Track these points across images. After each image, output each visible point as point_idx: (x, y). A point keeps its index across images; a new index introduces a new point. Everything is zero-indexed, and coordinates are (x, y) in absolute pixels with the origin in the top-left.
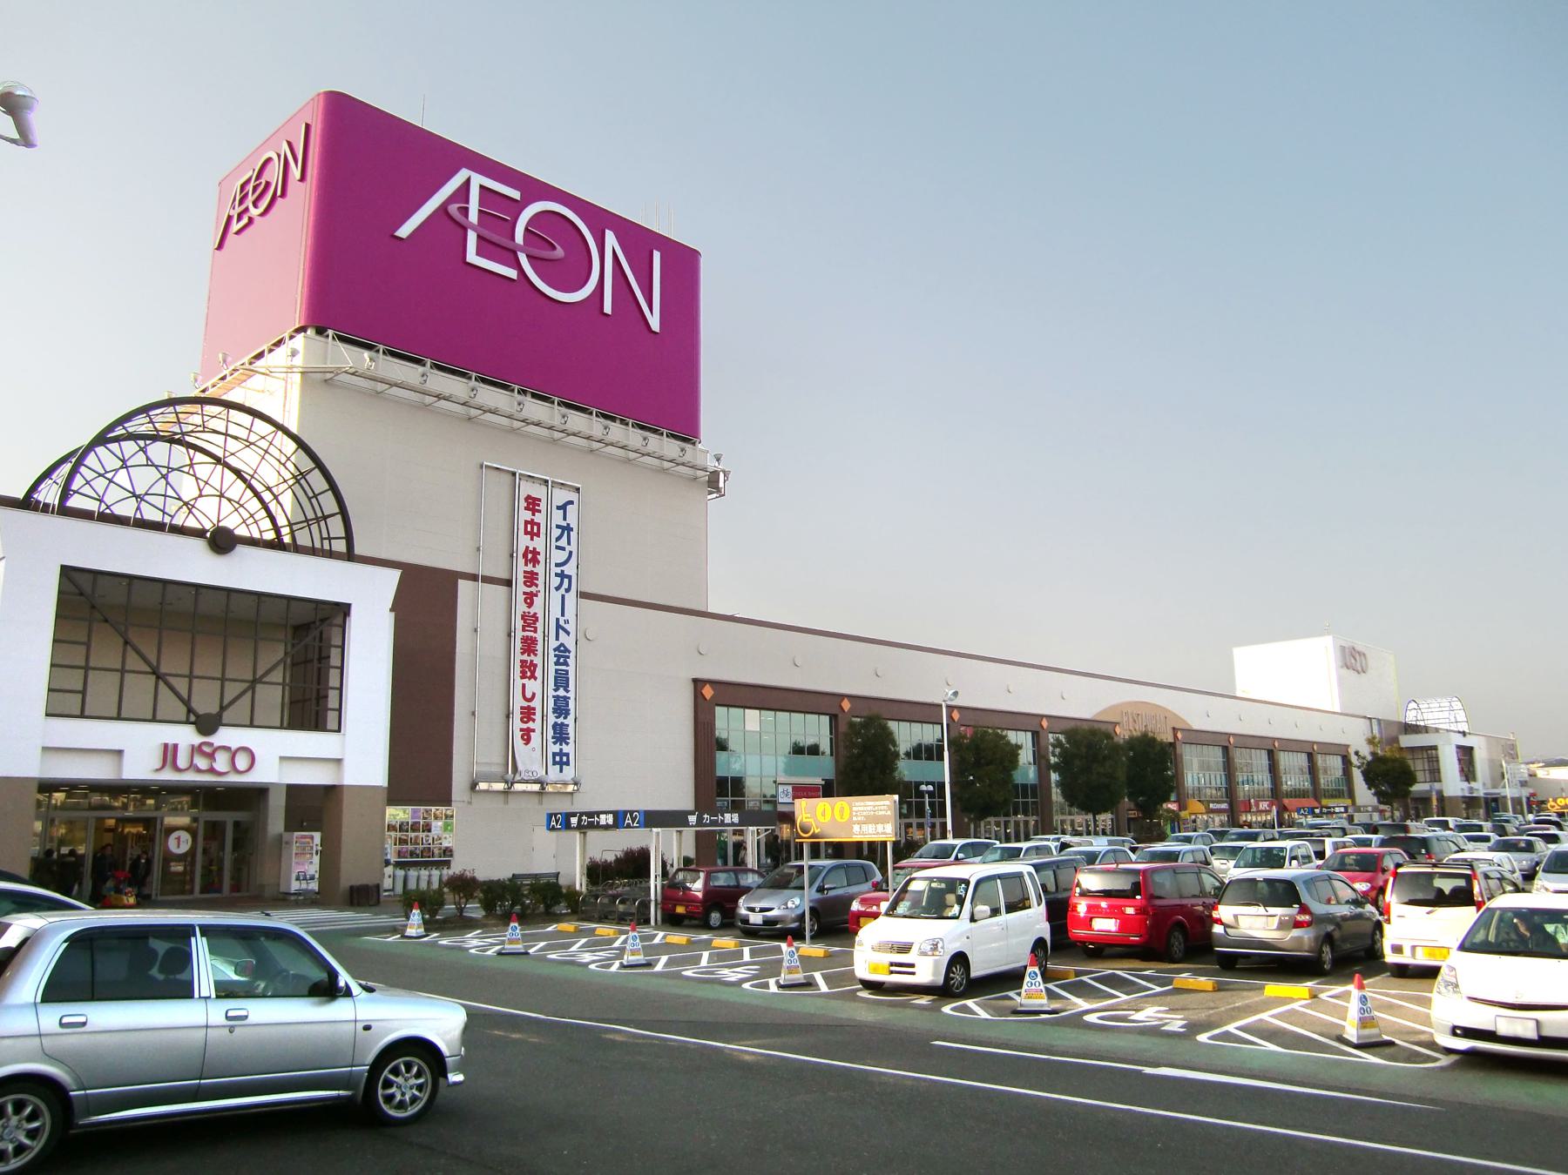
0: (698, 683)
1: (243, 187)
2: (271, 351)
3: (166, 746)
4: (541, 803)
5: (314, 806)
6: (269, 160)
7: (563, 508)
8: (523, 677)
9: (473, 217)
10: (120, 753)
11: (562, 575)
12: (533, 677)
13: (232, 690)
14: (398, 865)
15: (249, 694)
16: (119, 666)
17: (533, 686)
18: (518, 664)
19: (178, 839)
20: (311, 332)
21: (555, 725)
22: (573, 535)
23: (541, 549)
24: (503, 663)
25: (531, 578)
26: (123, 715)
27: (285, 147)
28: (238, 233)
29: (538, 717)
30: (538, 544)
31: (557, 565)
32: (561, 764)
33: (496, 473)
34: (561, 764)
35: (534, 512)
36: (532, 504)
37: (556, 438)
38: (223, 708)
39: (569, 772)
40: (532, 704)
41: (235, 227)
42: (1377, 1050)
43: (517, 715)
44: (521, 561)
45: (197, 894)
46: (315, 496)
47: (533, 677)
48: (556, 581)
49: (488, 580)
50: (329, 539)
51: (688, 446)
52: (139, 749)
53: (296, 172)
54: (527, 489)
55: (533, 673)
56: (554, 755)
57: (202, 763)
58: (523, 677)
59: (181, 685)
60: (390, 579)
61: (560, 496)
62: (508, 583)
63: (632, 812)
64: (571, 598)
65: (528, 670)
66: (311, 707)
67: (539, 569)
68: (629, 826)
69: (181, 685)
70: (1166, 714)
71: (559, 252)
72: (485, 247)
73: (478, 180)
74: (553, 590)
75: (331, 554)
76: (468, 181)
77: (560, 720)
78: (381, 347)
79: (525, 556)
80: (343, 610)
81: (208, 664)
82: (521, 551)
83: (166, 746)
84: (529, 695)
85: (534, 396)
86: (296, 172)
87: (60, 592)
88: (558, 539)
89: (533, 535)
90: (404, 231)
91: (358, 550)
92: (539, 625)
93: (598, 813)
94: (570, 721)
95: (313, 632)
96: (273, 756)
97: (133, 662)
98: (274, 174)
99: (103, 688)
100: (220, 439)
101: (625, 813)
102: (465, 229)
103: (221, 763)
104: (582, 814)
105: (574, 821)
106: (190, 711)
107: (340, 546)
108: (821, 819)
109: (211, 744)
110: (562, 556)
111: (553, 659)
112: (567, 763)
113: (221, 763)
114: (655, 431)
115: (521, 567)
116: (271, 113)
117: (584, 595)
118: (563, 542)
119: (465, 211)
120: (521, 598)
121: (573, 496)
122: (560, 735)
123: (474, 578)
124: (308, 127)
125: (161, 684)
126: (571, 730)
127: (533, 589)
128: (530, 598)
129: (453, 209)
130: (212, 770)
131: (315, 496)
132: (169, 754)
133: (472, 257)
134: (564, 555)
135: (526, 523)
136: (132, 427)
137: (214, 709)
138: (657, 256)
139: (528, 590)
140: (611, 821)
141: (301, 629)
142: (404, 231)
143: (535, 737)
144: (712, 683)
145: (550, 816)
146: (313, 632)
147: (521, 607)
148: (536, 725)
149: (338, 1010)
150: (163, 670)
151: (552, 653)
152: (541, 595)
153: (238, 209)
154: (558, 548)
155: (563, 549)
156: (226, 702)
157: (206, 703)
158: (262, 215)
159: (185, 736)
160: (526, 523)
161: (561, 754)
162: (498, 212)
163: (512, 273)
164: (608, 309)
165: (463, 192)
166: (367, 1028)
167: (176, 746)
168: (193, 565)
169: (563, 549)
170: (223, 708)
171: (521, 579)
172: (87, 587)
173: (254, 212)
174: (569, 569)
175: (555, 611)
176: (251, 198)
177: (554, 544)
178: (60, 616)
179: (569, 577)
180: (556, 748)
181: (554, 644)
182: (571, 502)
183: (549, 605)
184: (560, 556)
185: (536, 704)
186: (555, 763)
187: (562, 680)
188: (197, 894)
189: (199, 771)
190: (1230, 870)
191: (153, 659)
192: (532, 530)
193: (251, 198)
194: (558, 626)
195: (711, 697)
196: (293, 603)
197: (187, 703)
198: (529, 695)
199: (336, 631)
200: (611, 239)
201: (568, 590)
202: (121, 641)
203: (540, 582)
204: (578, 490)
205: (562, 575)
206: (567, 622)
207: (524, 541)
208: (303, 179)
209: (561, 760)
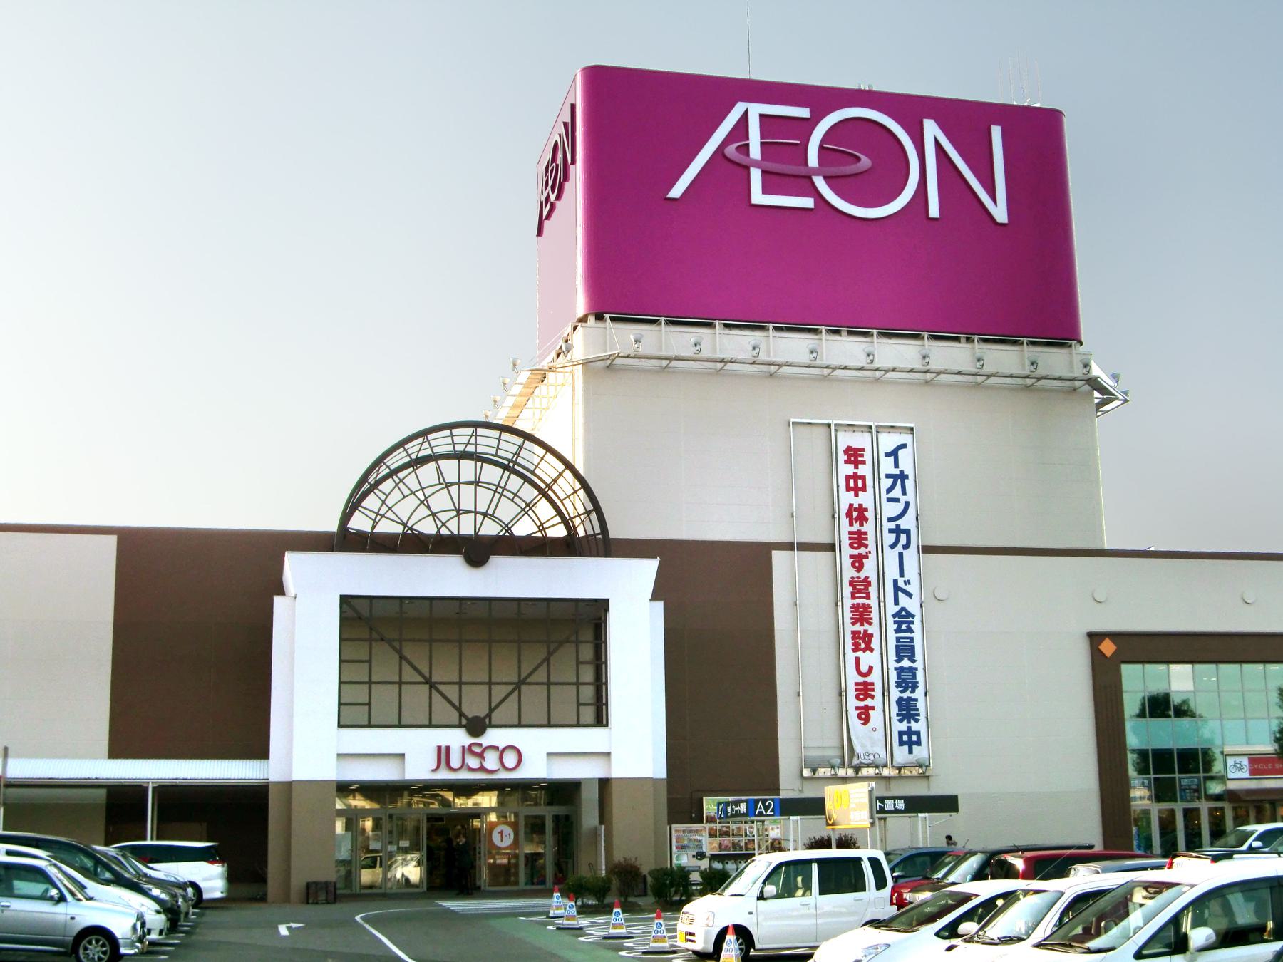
0: (1095, 638)
3: (439, 748)
7: (894, 454)
8: (856, 648)
9: (755, 152)
10: (403, 755)
11: (898, 531)
12: (869, 648)
13: (499, 692)
15: (516, 692)
16: (396, 679)
17: (868, 659)
18: (848, 636)
19: (501, 833)
20: (591, 319)
21: (900, 701)
24: (832, 634)
25: (858, 539)
26: (434, 722)
29: (877, 692)
30: (865, 499)
31: (890, 520)
32: (910, 744)
33: (809, 427)
34: (910, 744)
36: (854, 455)
38: (491, 710)
39: (920, 752)
40: (869, 679)
43: (851, 693)
45: (522, 885)
47: (869, 648)
49: (804, 547)
52: (416, 752)
54: (846, 440)
56: (901, 734)
57: (473, 762)
58: (854, 651)
59: (452, 692)
60: (648, 569)
61: (888, 442)
62: (831, 547)
64: (911, 556)
65: (862, 642)
67: (869, 527)
69: (452, 692)
71: (865, 162)
73: (756, 110)
74: (886, 548)
76: (746, 111)
77: (907, 695)
79: (849, 514)
81: (475, 669)
83: (439, 748)
84: (864, 669)
88: (889, 491)
90: (677, 191)
92: (873, 590)
94: (919, 694)
96: (541, 752)
97: (409, 674)
102: (747, 168)
103: (491, 761)
106: (461, 715)
109: (480, 745)
110: (896, 509)
111: (892, 627)
112: (918, 743)
113: (491, 761)
115: (845, 527)
116: (548, 103)
117: (927, 549)
118: (897, 493)
119: (745, 149)
120: (847, 562)
121: (906, 438)
122: (908, 710)
123: (789, 546)
126: (921, 705)
127: (863, 551)
128: (858, 562)
129: (731, 150)
130: (482, 769)
132: (443, 754)
133: (758, 197)
135: (848, 478)
137: (482, 712)
138: (996, 132)
139: (856, 552)
142: (677, 191)
143: (876, 716)
144: (1114, 636)
147: (849, 573)
148: (877, 702)
149: (61, 908)
151: (890, 620)
152: (872, 556)
154: (889, 500)
155: (897, 500)
159: (457, 738)
160: (848, 478)
161: (909, 732)
163: (808, 203)
164: (934, 211)
165: (742, 126)
166: (73, 918)
167: (448, 748)
168: (446, 578)
169: (897, 500)
170: (491, 710)
171: (846, 541)
172: (365, 612)
174: (904, 523)
175: (892, 572)
177: (884, 496)
179: (908, 532)
180: (903, 726)
181: (892, 609)
182: (904, 446)
183: (884, 566)
184: (892, 510)
185: (875, 678)
186: (901, 743)
188: (522, 885)
189: (470, 769)
191: (425, 671)
192: (856, 482)
194: (897, 589)
195: (1112, 654)
196: (552, 604)
197: (459, 709)
198: (864, 669)
200: (931, 129)
201: (906, 547)
202: (397, 657)
204: (912, 429)
205: (898, 531)
206: (907, 582)
207: (847, 498)
209: (910, 740)
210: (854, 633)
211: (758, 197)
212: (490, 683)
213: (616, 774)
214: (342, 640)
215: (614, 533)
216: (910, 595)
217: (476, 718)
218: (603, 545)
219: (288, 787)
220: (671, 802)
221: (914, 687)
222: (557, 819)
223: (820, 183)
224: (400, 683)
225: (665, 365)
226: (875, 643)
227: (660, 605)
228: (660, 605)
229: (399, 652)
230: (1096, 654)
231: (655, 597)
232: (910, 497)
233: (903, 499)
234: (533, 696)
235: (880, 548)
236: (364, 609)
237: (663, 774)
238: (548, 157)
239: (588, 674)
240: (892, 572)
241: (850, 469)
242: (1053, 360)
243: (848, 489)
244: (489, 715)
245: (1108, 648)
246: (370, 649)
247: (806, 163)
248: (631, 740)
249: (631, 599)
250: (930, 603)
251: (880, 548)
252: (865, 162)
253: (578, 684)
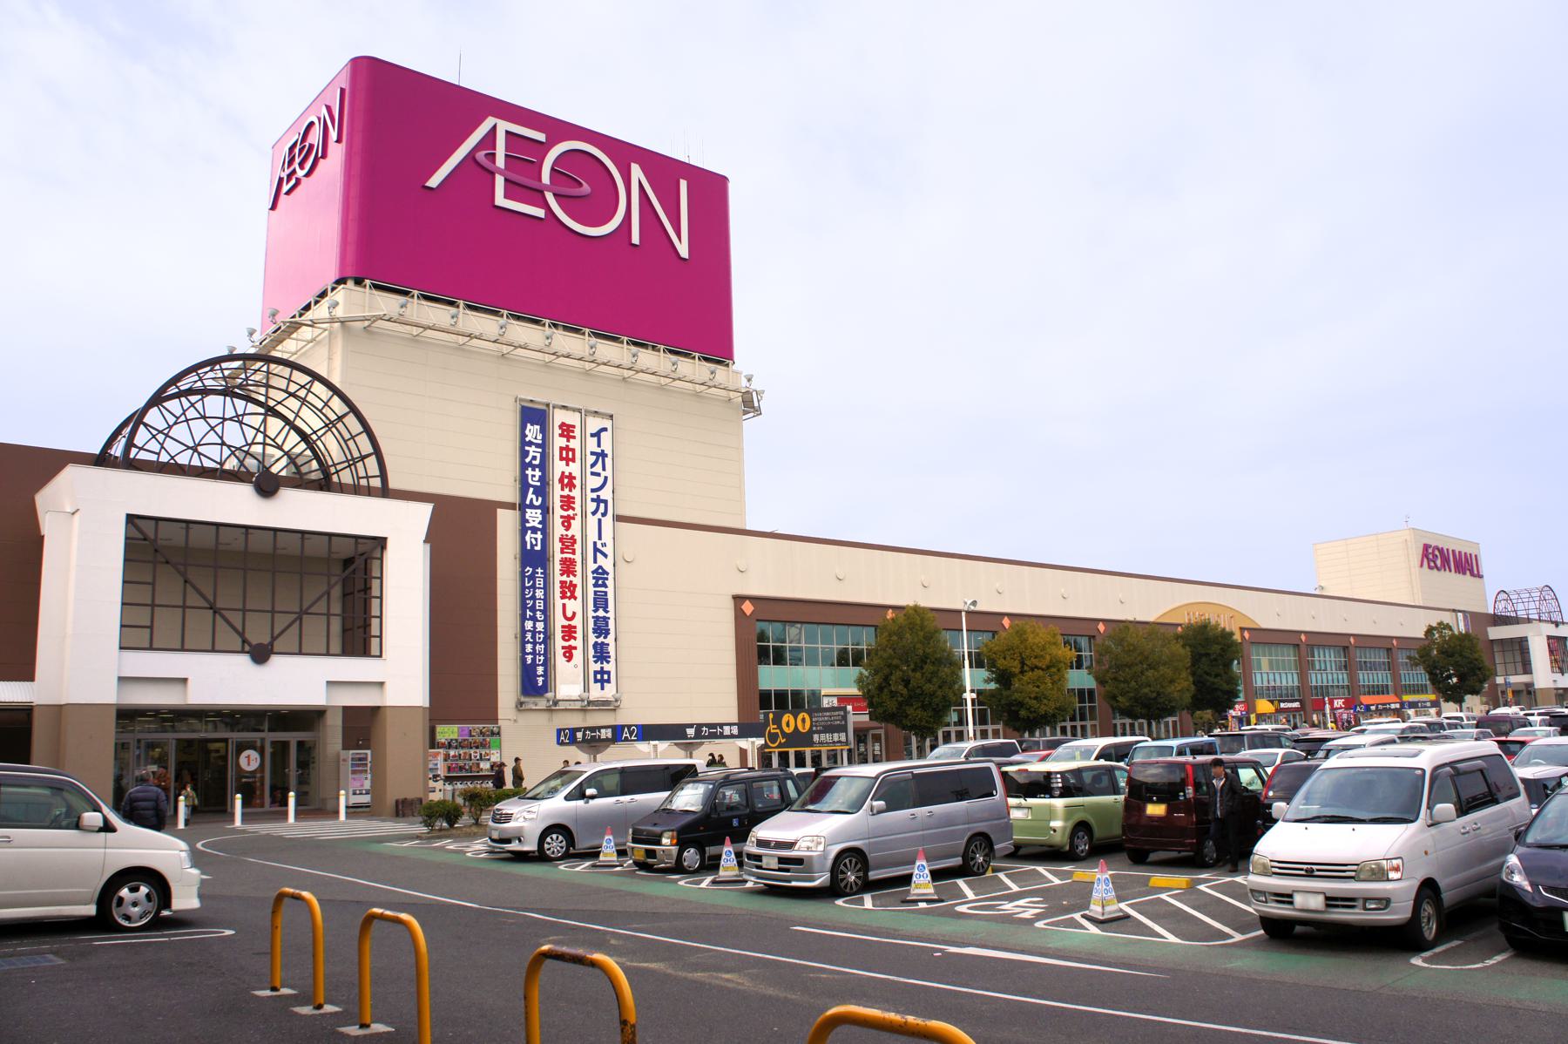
0: (739, 599)
1: (292, 149)
2: (317, 302)
4: (550, 720)
5: (363, 725)
6: (312, 124)
7: (597, 435)
9: (500, 162)
11: (598, 500)
12: (573, 597)
14: (448, 779)
17: (573, 606)
20: (350, 284)
21: (595, 645)
22: (608, 461)
23: (577, 473)
25: (568, 502)
27: (324, 111)
28: (288, 193)
29: (579, 635)
30: (574, 469)
31: (593, 491)
35: (569, 438)
36: (567, 430)
37: (590, 369)
38: (274, 638)
39: (609, 692)
40: (572, 623)
41: (285, 188)
42: (1114, 924)
43: (559, 634)
44: (557, 486)
45: (267, 807)
46: (353, 437)
47: (573, 597)
48: (592, 506)
50: (367, 477)
51: (720, 369)
53: (333, 135)
55: (573, 593)
59: (236, 618)
60: (422, 513)
61: (594, 424)
63: (629, 727)
64: (608, 522)
66: (358, 635)
67: (576, 493)
68: (626, 739)
69: (236, 618)
70: (1234, 614)
71: (586, 188)
72: (512, 190)
73: (503, 126)
74: (589, 515)
75: (369, 492)
76: (495, 127)
77: (600, 640)
78: (416, 292)
79: (561, 481)
80: (381, 543)
82: (557, 476)
84: (569, 615)
85: (565, 329)
86: (333, 135)
87: (127, 538)
88: (593, 466)
89: (568, 460)
90: (434, 181)
91: (393, 484)
92: (578, 547)
93: (600, 728)
94: (610, 640)
95: (357, 562)
96: (299, 680)
98: (315, 138)
99: (167, 622)
100: (262, 390)
101: (623, 727)
102: (493, 174)
104: (586, 729)
105: (579, 735)
107: (376, 483)
108: (786, 730)
110: (597, 482)
111: (591, 582)
112: (608, 681)
114: (686, 355)
117: (619, 518)
118: (598, 468)
119: (492, 157)
120: (558, 521)
121: (607, 423)
122: (601, 654)
124: (343, 91)
125: (218, 617)
126: (611, 649)
127: (571, 512)
128: (567, 522)
129: (481, 155)
131: (353, 437)
133: (500, 200)
134: (601, 480)
135: (562, 449)
136: (184, 385)
137: (266, 640)
138: (683, 184)
140: (610, 735)
141: (348, 562)
142: (434, 181)
143: (578, 655)
144: (754, 599)
145: (559, 731)
146: (357, 562)
148: (578, 643)
150: (219, 605)
151: (590, 576)
152: (578, 518)
153: (287, 171)
154: (593, 474)
156: (277, 632)
157: (258, 636)
158: (308, 175)
160: (562, 449)
161: (602, 672)
162: (524, 155)
163: (540, 213)
164: (636, 239)
168: (235, 505)
170: (274, 638)
171: (558, 503)
173: (300, 173)
174: (605, 494)
175: (592, 535)
176: (297, 160)
177: (589, 470)
178: (127, 560)
179: (606, 502)
180: (597, 667)
181: (592, 567)
182: (605, 429)
184: (595, 482)
185: (577, 622)
186: (596, 681)
187: (601, 602)
188: (267, 807)
190: (729, 750)
193: (297, 160)
194: (596, 550)
197: (242, 634)
198: (569, 615)
199: (376, 563)
200: (636, 172)
201: (604, 515)
203: (577, 506)
204: (611, 417)
205: (598, 500)
206: (604, 545)
208: (339, 141)
209: (602, 678)
210: (562, 582)
214: (126, 560)
216: (605, 556)
217: (260, 645)
219: (58, 711)
221: (607, 633)
223: (550, 197)
224: (184, 607)
226: (578, 593)
229: (183, 574)
230: (739, 614)
232: (608, 473)
233: (603, 474)
236: (149, 528)
240: (592, 535)
243: (562, 459)
244: (271, 644)
245: (748, 608)
246: (216, 576)
247: (540, 179)
248: (400, 671)
252: (586, 188)
253: (328, 615)
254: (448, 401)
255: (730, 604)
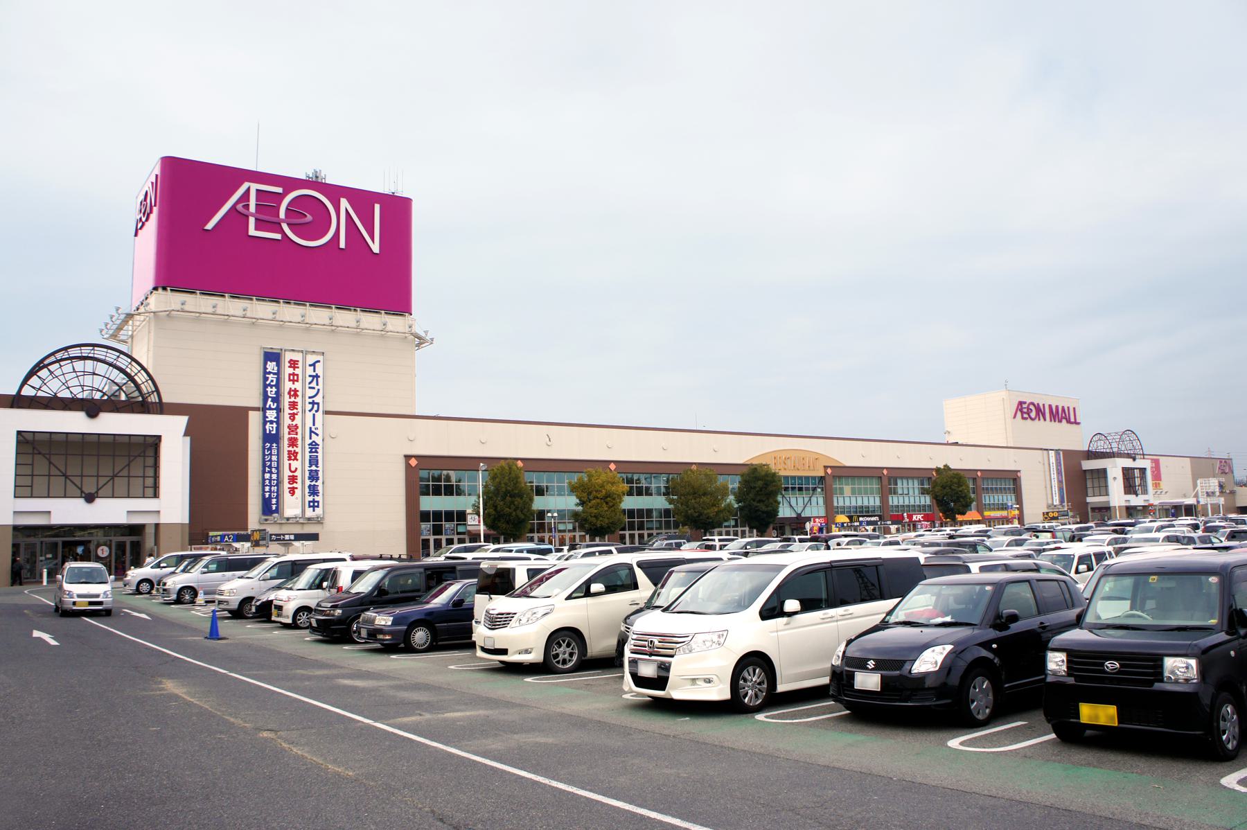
0: (408, 457)
7: (313, 365)
8: (290, 459)
9: (252, 209)
12: (296, 459)
13: (102, 481)
17: (295, 464)
29: (299, 480)
30: (298, 386)
32: (314, 507)
34: (314, 507)
36: (293, 364)
39: (319, 511)
43: (286, 480)
47: (296, 459)
60: (182, 421)
61: (311, 359)
64: (319, 416)
67: (299, 400)
69: (77, 481)
71: (309, 218)
73: (254, 187)
90: (210, 226)
92: (299, 431)
94: (319, 483)
97: (54, 471)
110: (313, 392)
117: (327, 413)
118: (314, 384)
119: (247, 207)
121: (320, 358)
122: (314, 491)
126: (320, 489)
128: (293, 416)
129: (240, 207)
133: (252, 231)
138: (377, 207)
142: (210, 226)
143: (298, 492)
144: (416, 457)
148: (298, 485)
161: (314, 501)
162: (268, 203)
163: (278, 236)
164: (342, 245)
168: (75, 423)
174: (316, 400)
175: (309, 423)
180: (311, 498)
181: (308, 441)
185: (298, 473)
194: (311, 432)
200: (344, 203)
205: (313, 403)
209: (314, 505)
211: (252, 231)
212: (98, 476)
213: (162, 521)
215: (165, 400)
218: (161, 408)
220: (190, 534)
221: (317, 479)
222: (132, 543)
223: (285, 227)
225: (198, 317)
226: (299, 457)
227: (188, 439)
228: (188, 439)
229: (49, 460)
230: (408, 466)
231: (185, 435)
232: (320, 386)
234: (120, 483)
235: (304, 411)
236: (30, 437)
237: (187, 521)
238: (142, 197)
239: (150, 472)
241: (291, 371)
242: (395, 323)
245: (413, 462)
248: (172, 503)
249: (173, 435)
250: (328, 439)
251: (304, 411)
252: (309, 218)
254: (212, 352)
255: (403, 460)
